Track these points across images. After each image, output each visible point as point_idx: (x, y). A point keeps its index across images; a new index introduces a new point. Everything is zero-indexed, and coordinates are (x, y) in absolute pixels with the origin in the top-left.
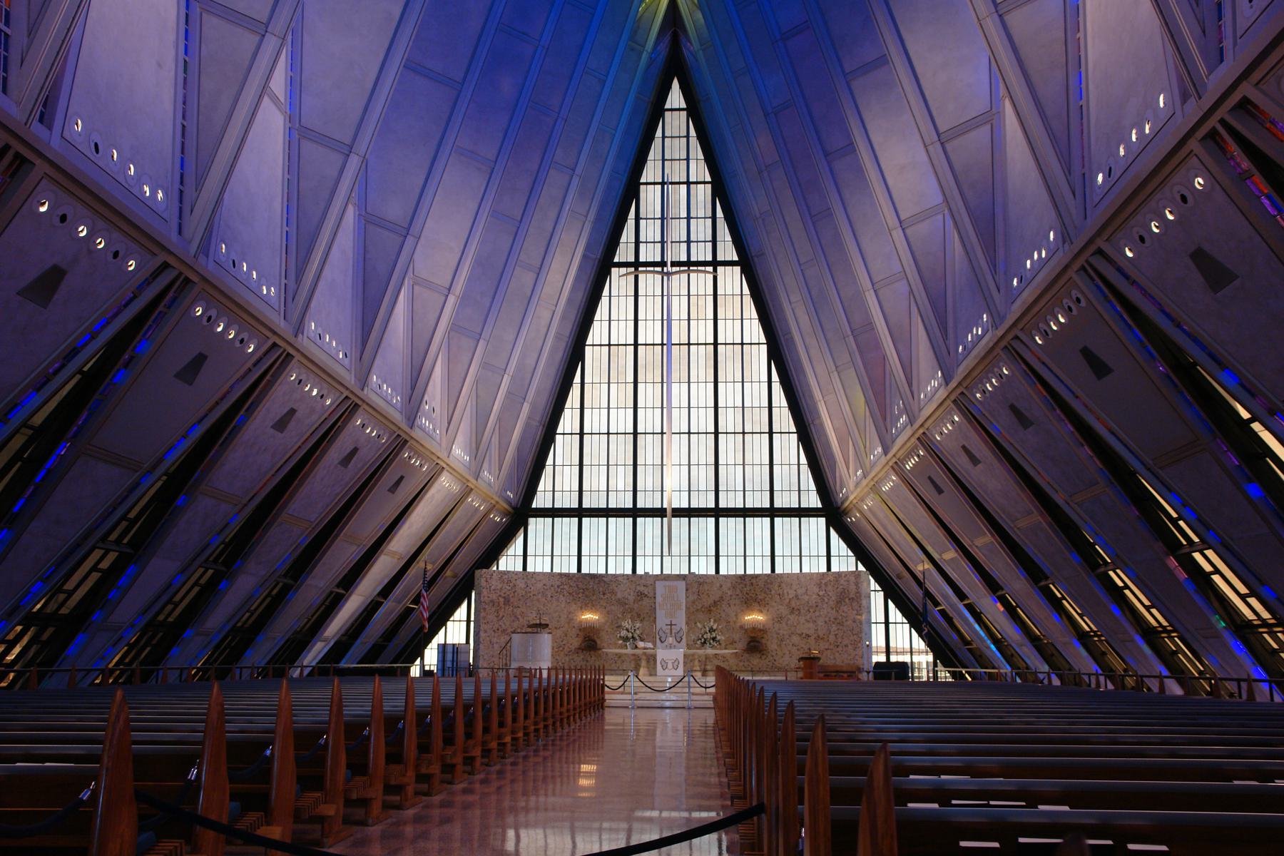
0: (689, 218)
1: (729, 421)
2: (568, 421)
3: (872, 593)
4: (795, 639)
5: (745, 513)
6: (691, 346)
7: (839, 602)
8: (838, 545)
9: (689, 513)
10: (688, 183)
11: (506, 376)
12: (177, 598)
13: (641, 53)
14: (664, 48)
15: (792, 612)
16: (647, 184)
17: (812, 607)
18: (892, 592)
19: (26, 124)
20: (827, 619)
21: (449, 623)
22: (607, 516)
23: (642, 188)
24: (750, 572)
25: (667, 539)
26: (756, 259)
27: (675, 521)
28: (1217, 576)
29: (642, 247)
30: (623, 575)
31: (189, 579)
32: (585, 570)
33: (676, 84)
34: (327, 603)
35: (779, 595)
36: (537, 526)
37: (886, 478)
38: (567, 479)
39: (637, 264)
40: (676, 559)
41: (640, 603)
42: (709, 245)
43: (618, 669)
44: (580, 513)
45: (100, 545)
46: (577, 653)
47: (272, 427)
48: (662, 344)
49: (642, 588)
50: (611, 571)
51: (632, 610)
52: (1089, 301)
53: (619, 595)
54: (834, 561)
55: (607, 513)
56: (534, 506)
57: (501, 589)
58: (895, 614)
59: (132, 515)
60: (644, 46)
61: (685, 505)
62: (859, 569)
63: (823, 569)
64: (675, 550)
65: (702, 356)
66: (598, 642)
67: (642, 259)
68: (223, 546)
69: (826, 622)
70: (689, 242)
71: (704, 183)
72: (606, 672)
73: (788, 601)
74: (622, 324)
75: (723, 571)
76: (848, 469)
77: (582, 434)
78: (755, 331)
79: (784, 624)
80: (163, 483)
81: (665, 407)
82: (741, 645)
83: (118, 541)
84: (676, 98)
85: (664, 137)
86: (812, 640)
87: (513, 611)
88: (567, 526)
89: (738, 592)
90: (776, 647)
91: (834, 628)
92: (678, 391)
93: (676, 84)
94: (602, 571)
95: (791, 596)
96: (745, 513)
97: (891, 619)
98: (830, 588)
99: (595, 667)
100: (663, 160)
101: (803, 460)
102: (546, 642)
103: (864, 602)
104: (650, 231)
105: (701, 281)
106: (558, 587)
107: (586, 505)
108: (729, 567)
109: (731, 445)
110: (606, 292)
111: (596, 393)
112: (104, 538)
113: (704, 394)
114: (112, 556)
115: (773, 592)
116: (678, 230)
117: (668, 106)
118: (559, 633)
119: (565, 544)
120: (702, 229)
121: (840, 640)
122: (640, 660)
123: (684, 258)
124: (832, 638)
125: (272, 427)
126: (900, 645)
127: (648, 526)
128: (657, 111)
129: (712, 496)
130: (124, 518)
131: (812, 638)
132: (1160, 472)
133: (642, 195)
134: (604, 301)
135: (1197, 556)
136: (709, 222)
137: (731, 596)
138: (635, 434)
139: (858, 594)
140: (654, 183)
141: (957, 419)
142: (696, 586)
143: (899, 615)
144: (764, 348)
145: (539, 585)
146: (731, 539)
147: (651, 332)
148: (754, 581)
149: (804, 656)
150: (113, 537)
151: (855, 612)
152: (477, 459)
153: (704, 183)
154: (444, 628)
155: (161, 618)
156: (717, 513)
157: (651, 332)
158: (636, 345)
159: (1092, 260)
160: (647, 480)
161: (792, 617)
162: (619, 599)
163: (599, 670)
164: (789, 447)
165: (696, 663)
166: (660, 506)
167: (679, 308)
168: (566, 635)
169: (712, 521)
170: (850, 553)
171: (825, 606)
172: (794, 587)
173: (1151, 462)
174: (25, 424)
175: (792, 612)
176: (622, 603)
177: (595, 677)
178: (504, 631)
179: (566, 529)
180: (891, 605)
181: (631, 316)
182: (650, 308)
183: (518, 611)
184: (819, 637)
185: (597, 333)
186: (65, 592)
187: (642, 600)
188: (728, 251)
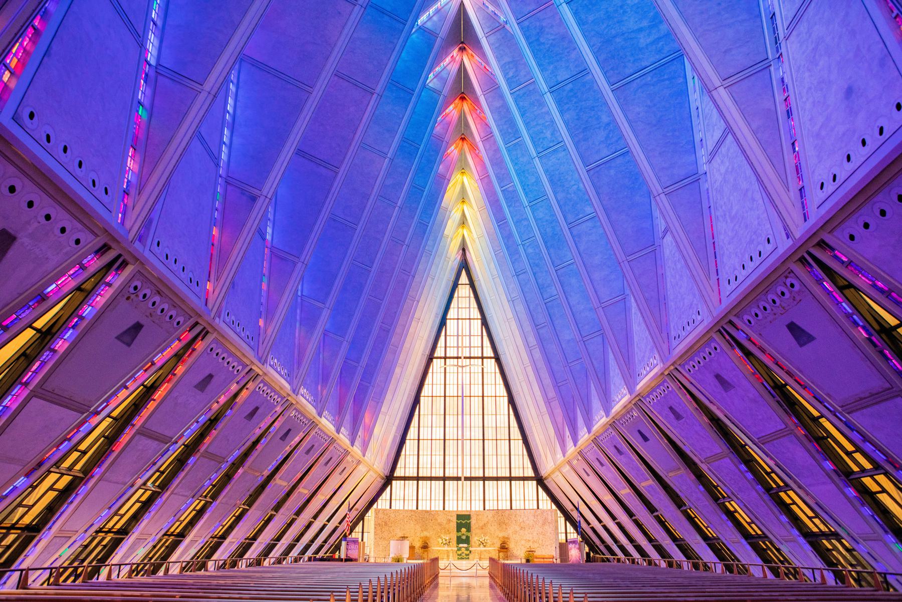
1: (489, 434)
2: (412, 433)
3: (559, 518)
4: (523, 542)
7: (544, 524)
12: (122, 512)
15: (521, 529)
19: (132, 242)
28: (795, 506)
29: (448, 349)
44: (418, 479)
49: (449, 518)
51: (445, 528)
52: (721, 348)
53: (439, 521)
56: (395, 475)
74: (438, 386)
83: (70, 468)
84: (464, 278)
85: (458, 297)
91: (541, 537)
97: (568, 531)
100: (458, 308)
104: (452, 341)
107: (420, 475)
111: (426, 419)
113: (477, 420)
114: (66, 479)
120: (476, 341)
124: (540, 542)
128: (455, 285)
132: (762, 445)
135: (782, 494)
149: (528, 550)
150: (66, 464)
155: (172, 530)
159: (725, 327)
164: (518, 446)
165: (477, 554)
170: (548, 498)
172: (522, 517)
173: (756, 440)
175: (521, 529)
176: (440, 524)
183: (391, 529)
185: (426, 391)
186: (25, 506)
188: (489, 352)
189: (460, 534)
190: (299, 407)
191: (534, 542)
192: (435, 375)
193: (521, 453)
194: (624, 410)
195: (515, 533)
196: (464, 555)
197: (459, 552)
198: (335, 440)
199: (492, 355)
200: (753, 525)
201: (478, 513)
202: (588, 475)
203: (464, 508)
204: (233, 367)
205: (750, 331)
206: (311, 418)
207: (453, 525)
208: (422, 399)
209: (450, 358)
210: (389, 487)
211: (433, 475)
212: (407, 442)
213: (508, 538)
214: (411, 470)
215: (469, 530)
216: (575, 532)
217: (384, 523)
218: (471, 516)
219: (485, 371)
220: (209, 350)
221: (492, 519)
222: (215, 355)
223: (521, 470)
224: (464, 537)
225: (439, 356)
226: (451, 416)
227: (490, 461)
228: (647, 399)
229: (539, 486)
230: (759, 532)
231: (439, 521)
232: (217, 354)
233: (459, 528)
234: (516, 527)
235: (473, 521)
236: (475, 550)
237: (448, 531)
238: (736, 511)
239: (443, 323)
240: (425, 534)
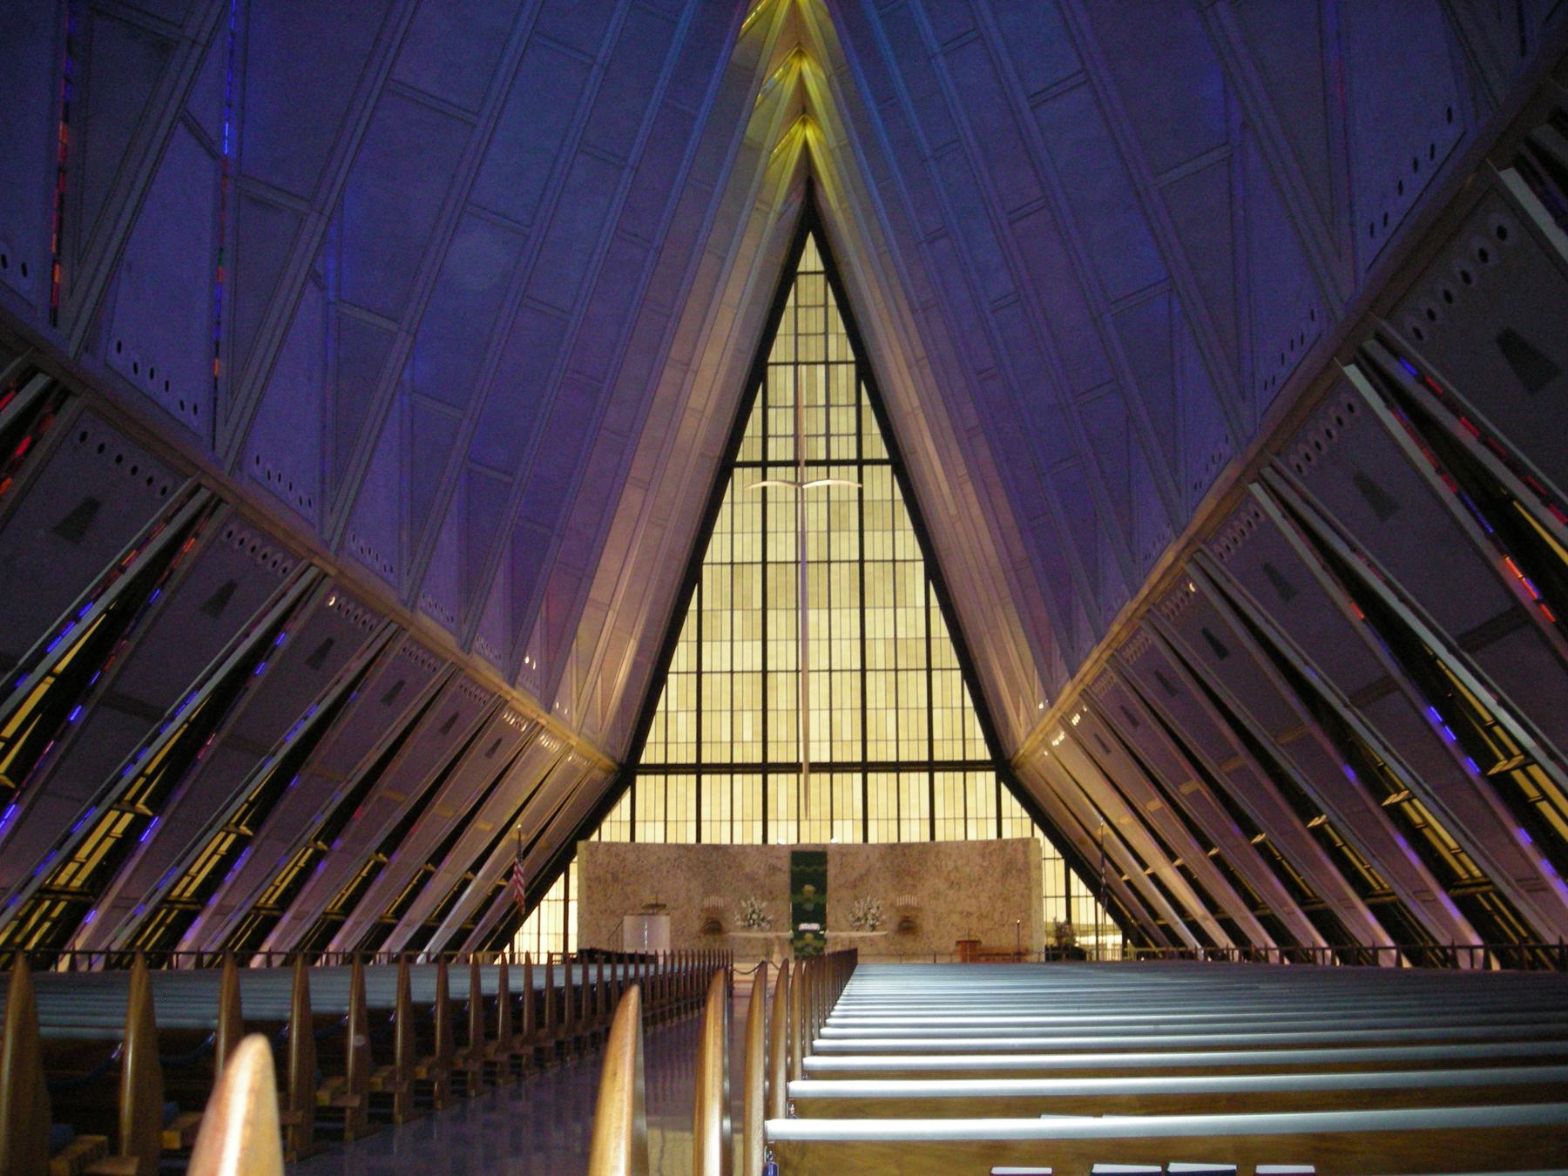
0: (828, 406)
1: (879, 655)
2: (683, 657)
4: (955, 918)
5: (898, 767)
6: (832, 565)
7: (1005, 874)
8: (1011, 803)
9: (832, 768)
10: (827, 363)
11: (610, 613)
13: (768, 214)
14: (796, 205)
16: (776, 364)
17: (974, 880)
18: (1074, 860)
20: (991, 894)
21: (542, 903)
22: (732, 773)
23: (771, 369)
24: (904, 839)
25: (802, 797)
26: (909, 456)
27: (814, 777)
30: (752, 846)
31: (205, 848)
32: (705, 840)
33: (811, 242)
34: (414, 882)
35: (936, 866)
36: (646, 785)
37: (1054, 732)
38: (683, 726)
39: (764, 464)
40: (816, 824)
41: (773, 878)
42: (853, 440)
43: (748, 955)
44: (698, 769)
45: (115, 806)
46: (699, 937)
47: (382, 701)
48: (797, 562)
49: (774, 861)
50: (737, 841)
53: (748, 869)
54: (1006, 824)
55: (731, 769)
56: (642, 761)
57: (609, 863)
58: (1079, 886)
59: (149, 770)
60: (771, 206)
61: (826, 759)
62: (1036, 836)
63: (993, 835)
64: (814, 812)
65: (844, 576)
66: (724, 925)
67: (771, 457)
68: (246, 805)
69: (990, 898)
70: (828, 435)
71: (847, 363)
72: (735, 958)
75: (872, 839)
76: (1018, 716)
77: (699, 673)
78: (909, 546)
79: (942, 900)
80: (50, 689)
81: (802, 639)
82: (893, 925)
84: (811, 259)
85: (796, 306)
86: (974, 920)
87: (622, 889)
88: (683, 785)
89: (888, 864)
90: (933, 928)
91: (1000, 904)
92: (816, 618)
93: (811, 242)
94: (726, 841)
95: (950, 869)
96: (898, 767)
97: (1074, 892)
98: (994, 858)
99: (686, 951)
100: (797, 335)
101: (969, 702)
102: (664, 922)
103: (1034, 874)
104: (781, 422)
105: (843, 481)
106: (675, 860)
107: (705, 759)
108: (880, 834)
109: (881, 684)
110: (727, 498)
112: (120, 799)
115: (929, 864)
116: (814, 422)
117: (801, 268)
118: (677, 914)
119: (681, 807)
120: (844, 420)
121: (1006, 918)
122: (773, 945)
123: (822, 456)
124: (997, 916)
125: (382, 701)
126: (1083, 921)
127: (782, 785)
128: (789, 275)
129: (858, 747)
130: (141, 774)
131: (975, 916)
133: (771, 379)
134: (725, 509)
136: (853, 411)
137: (880, 868)
138: (765, 672)
139: (1027, 864)
140: (785, 364)
141: (1085, 710)
143: (1083, 887)
144: (920, 566)
145: (653, 859)
146: (882, 799)
147: (782, 548)
148: (906, 851)
151: (1023, 886)
152: (580, 708)
153: (847, 363)
154: (537, 908)
156: (865, 767)
157: (782, 548)
158: (764, 563)
160: (781, 728)
161: (951, 893)
162: (747, 874)
163: (704, 956)
164: (951, 686)
166: (795, 761)
167: (816, 516)
168: (685, 917)
169: (858, 777)
170: (1025, 814)
171: (989, 879)
174: (50, 673)
176: (750, 878)
177: (687, 965)
178: (613, 912)
179: (681, 789)
180: (1073, 875)
181: (759, 527)
182: (780, 518)
183: (629, 889)
184: (982, 915)
185: (717, 549)
187: (774, 874)
188: (876, 447)
189: (799, 898)
190: (471, 672)
191: (981, 917)
192: (737, 509)
193: (958, 703)
194: (1168, 580)
195: (937, 895)
196: (810, 949)
197: (799, 944)
198: (507, 702)
199: (885, 456)
200: (1463, 857)
201: (844, 850)
202: (1108, 751)
203: (815, 835)
204: (265, 557)
206: (496, 689)
207: (784, 879)
209: (777, 464)
211: (738, 759)
212: (671, 678)
213: (919, 909)
214: (682, 748)
215: (822, 888)
216: (1090, 893)
217: (609, 877)
218: (829, 858)
219: (866, 497)
220: (225, 533)
222: (237, 543)
224: (809, 907)
225: (748, 458)
226: (912, 704)
227: (882, 723)
228: (1215, 546)
229: (1003, 787)
230: (1477, 873)
231: (748, 869)
232: (241, 542)
233: (797, 883)
235: (832, 870)
236: (836, 938)
237: (771, 893)
238: (1427, 825)
239: (757, 375)
240: (714, 901)
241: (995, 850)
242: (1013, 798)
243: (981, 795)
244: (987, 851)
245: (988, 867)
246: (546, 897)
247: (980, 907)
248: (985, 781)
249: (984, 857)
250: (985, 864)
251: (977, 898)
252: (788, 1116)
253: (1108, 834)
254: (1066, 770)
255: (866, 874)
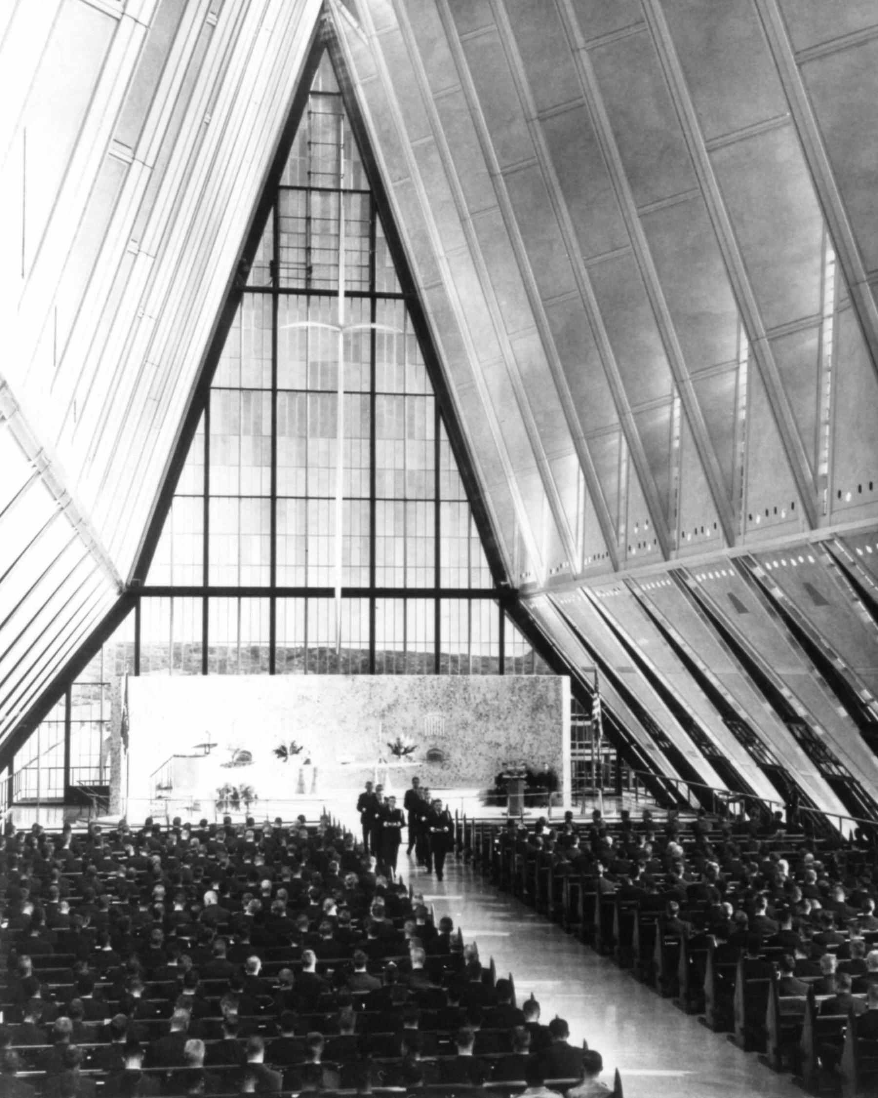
4: (483, 748)
20: (521, 727)
23: (283, 193)
35: (465, 699)
69: (519, 730)
73: (475, 705)
89: (416, 695)
95: (478, 701)
98: (524, 693)
104: (291, 256)
115: (457, 696)
121: (535, 751)
129: (366, 573)
131: (503, 747)
142: (367, 687)
144: (431, 401)
161: (480, 724)
169: (366, 602)
184: (511, 746)
188: (387, 281)
199: (398, 290)
205: (658, 282)
208: (215, 398)
210: (132, 614)
221: (407, 695)
223: (464, 573)
234: (466, 712)
241: (525, 686)
242: (516, 630)
243: (485, 621)
244: (517, 686)
245: (518, 701)
246: (47, 718)
247: (508, 739)
248: (489, 608)
249: (513, 692)
250: (514, 699)
251: (506, 729)
252: (573, 728)
253: (345, 158)
254: (192, 24)
255: (394, 705)
